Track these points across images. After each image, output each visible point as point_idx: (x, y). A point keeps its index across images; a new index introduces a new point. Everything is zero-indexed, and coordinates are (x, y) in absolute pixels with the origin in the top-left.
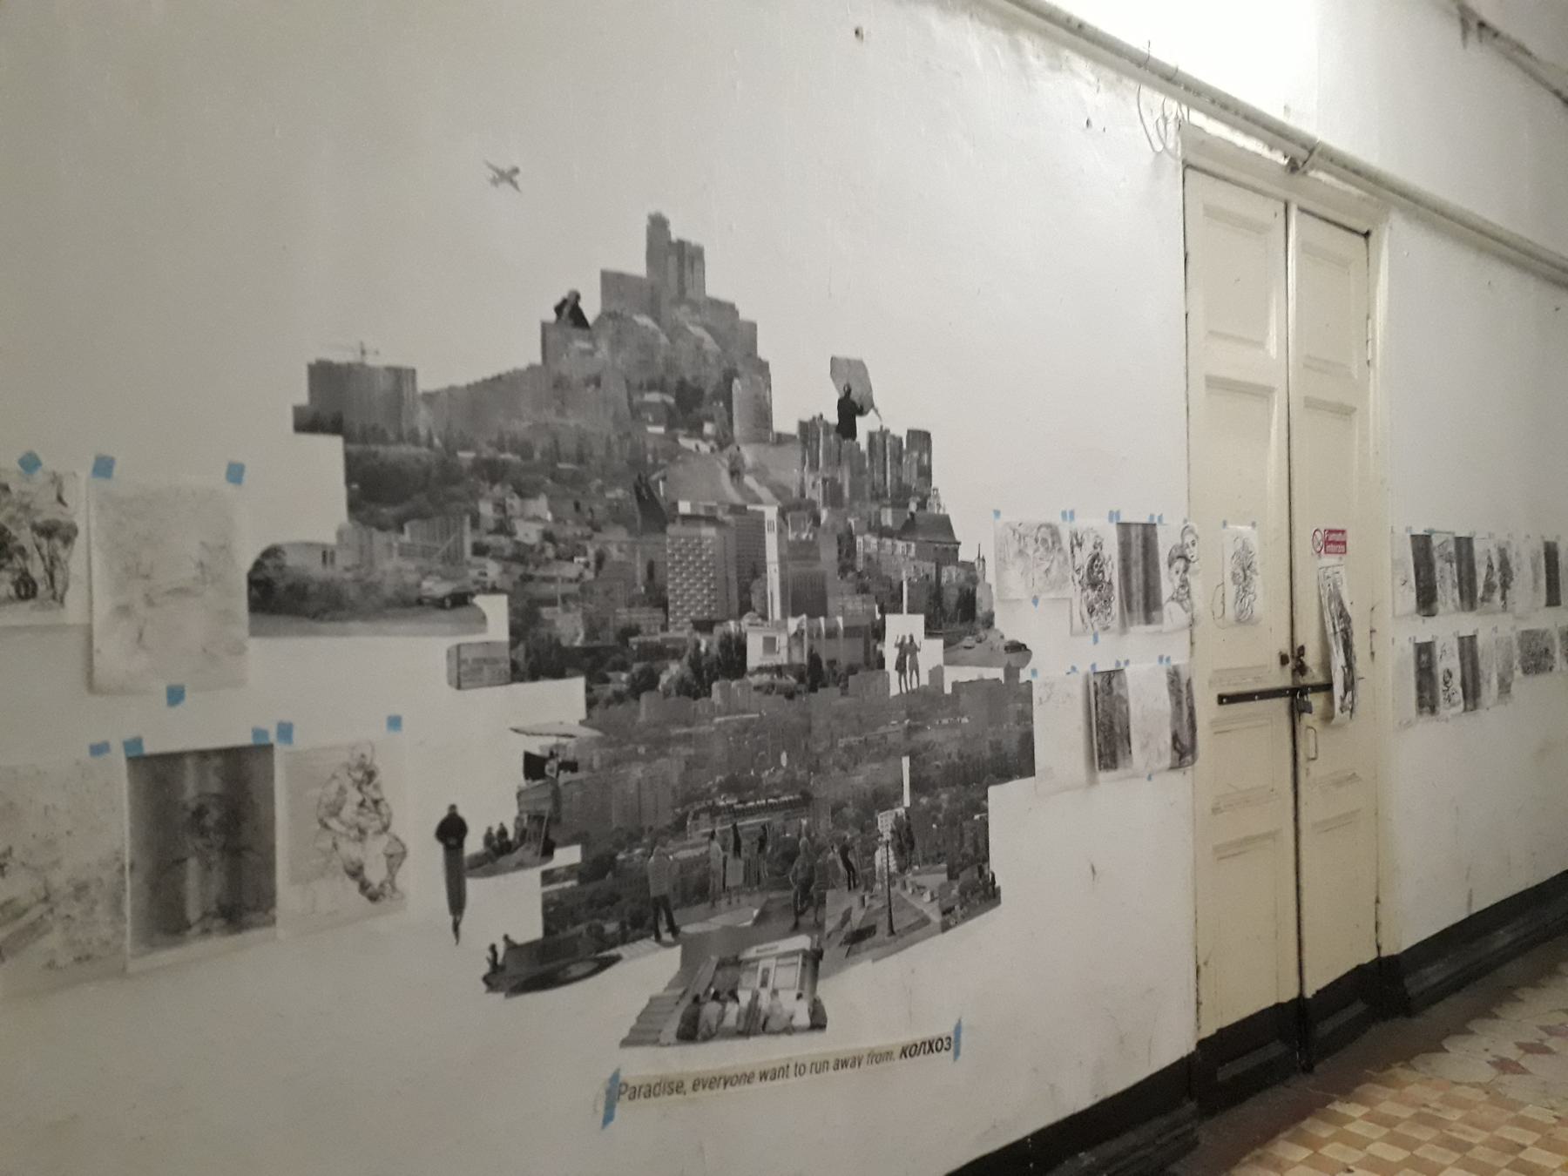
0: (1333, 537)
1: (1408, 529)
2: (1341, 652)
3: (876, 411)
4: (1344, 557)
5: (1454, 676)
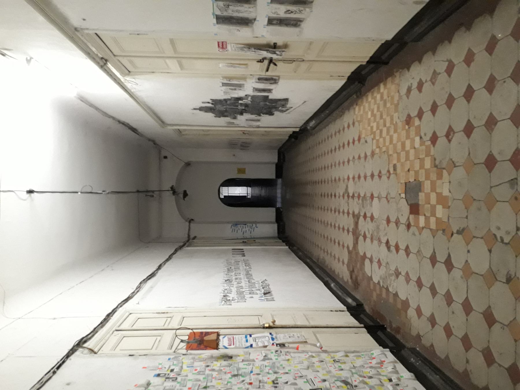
0: (221, 45)
1: (214, 25)
2: (262, 52)
3: (504, 283)
4: (228, 42)
5: (290, 9)
